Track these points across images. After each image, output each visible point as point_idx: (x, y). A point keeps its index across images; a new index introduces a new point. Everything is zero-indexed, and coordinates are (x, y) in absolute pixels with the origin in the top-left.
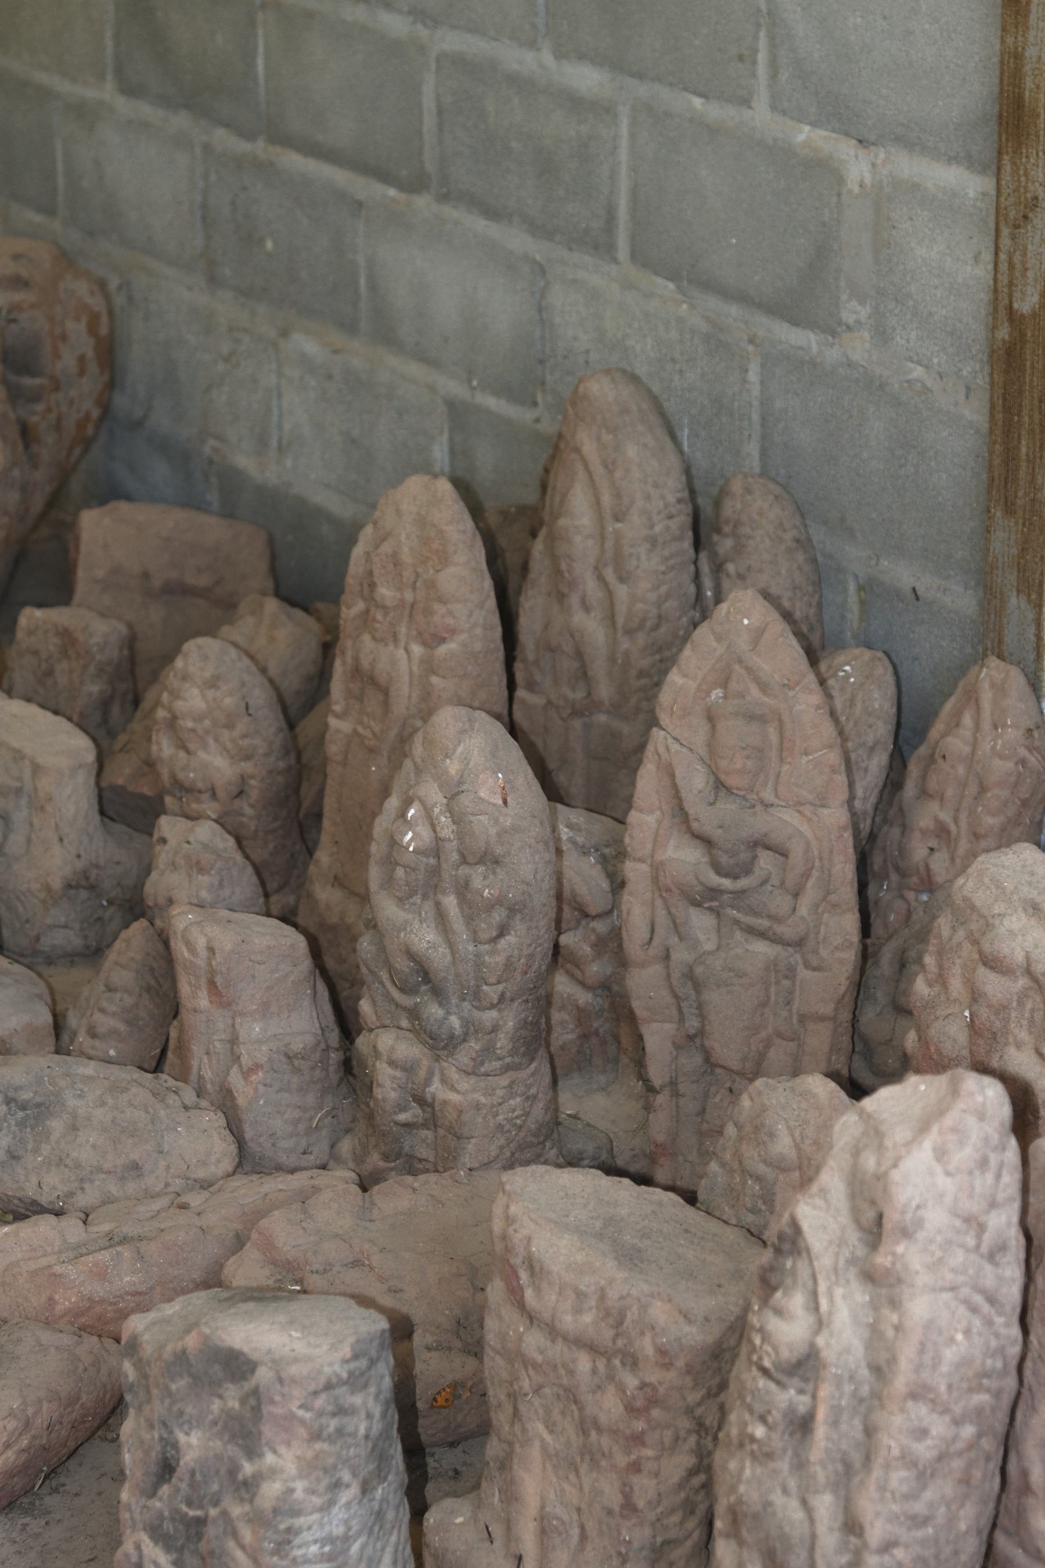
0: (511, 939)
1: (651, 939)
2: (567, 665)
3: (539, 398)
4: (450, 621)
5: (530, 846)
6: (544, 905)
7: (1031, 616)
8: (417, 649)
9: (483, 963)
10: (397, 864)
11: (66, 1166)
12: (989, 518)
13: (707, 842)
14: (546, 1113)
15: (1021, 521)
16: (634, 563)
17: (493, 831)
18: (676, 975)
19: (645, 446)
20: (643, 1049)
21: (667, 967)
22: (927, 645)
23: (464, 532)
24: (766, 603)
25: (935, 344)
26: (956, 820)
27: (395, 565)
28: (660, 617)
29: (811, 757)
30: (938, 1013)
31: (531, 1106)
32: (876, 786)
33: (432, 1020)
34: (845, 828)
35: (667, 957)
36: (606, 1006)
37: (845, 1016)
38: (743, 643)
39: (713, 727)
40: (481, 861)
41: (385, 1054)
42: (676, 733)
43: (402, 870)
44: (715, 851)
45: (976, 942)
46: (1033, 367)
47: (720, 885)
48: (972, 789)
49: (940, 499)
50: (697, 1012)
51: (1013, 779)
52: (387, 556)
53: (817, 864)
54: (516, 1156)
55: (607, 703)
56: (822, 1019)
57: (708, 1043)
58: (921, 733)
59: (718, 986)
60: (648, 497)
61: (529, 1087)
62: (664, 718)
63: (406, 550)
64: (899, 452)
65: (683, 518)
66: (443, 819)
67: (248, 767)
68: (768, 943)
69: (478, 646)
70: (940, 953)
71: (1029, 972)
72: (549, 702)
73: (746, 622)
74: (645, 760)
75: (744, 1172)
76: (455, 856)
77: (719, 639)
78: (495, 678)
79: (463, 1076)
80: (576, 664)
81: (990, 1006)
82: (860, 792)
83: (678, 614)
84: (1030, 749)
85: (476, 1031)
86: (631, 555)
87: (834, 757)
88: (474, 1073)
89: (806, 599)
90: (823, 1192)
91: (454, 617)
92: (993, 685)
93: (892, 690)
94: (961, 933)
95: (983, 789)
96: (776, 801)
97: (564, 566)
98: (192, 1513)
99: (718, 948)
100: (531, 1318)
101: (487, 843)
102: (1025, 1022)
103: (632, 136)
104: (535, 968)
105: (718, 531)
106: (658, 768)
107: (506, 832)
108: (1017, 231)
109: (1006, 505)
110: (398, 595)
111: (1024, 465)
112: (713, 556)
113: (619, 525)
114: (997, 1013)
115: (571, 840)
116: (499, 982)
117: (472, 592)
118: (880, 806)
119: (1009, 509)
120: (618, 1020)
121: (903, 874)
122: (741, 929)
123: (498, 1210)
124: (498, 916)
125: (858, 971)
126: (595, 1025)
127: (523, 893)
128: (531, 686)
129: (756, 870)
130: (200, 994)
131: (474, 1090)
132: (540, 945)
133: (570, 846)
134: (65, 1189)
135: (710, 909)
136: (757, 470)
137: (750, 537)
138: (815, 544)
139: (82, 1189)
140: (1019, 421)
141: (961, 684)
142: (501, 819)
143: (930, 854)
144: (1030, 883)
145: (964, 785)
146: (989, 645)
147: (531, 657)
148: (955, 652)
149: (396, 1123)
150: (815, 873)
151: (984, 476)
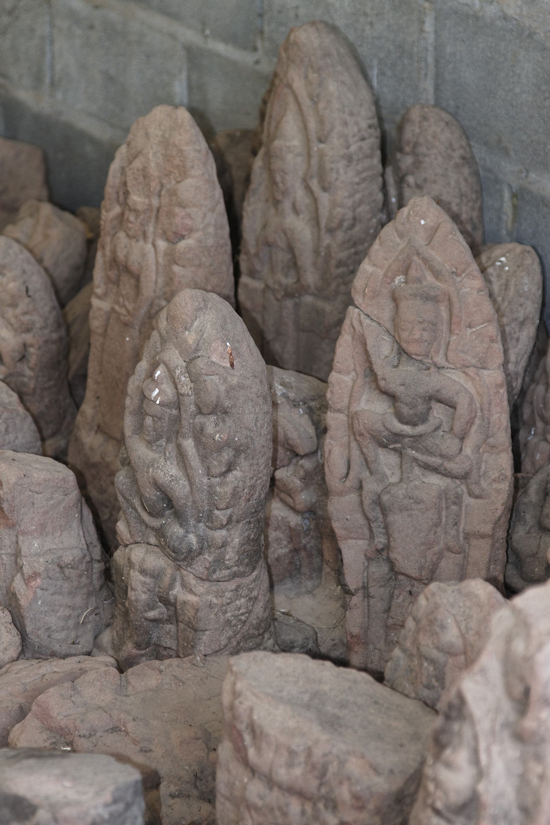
0: (237, 473)
1: (348, 473)
2: (282, 257)
4: (188, 222)
5: (252, 400)
6: (263, 446)
8: (162, 244)
9: (215, 492)
10: (147, 414)
13: (392, 397)
14: (265, 611)
16: (334, 175)
17: (222, 388)
18: (367, 502)
19: (343, 83)
20: (342, 560)
21: (361, 496)
23: (199, 151)
27: (144, 177)
28: (354, 219)
29: (474, 330)
32: (526, 353)
34: (501, 386)
35: (360, 487)
36: (312, 527)
37: (501, 534)
38: (420, 240)
39: (397, 306)
42: (368, 311)
43: (151, 418)
44: (398, 404)
50: (384, 531)
52: (138, 170)
53: (479, 414)
54: (241, 645)
57: (392, 556)
59: (401, 511)
60: (345, 124)
61: (251, 590)
62: (358, 299)
63: (153, 165)
65: (373, 140)
67: (28, 338)
69: (210, 242)
72: (267, 287)
73: (423, 222)
74: (343, 332)
75: (422, 657)
76: (193, 408)
78: (224, 268)
79: (199, 581)
83: (369, 216)
85: (209, 546)
86: (332, 169)
87: (492, 330)
88: (208, 580)
89: (470, 204)
90: (483, 671)
93: (538, 277)
96: (446, 364)
97: (278, 179)
99: (401, 480)
100: (253, 771)
101: (218, 397)
104: (255, 496)
107: (232, 389)
112: (397, 169)
113: (322, 146)
115: (284, 395)
116: (227, 508)
117: (206, 199)
118: (529, 369)
122: (419, 466)
123: (227, 686)
124: (227, 455)
125: (511, 499)
126: (304, 542)
128: (252, 274)
129: (431, 418)
131: (208, 593)
132: (260, 478)
133: (284, 400)
135: (395, 450)
136: (432, 102)
137: (425, 155)
138: (478, 160)
142: (229, 379)
147: (252, 251)
149: (146, 619)
150: (477, 421)
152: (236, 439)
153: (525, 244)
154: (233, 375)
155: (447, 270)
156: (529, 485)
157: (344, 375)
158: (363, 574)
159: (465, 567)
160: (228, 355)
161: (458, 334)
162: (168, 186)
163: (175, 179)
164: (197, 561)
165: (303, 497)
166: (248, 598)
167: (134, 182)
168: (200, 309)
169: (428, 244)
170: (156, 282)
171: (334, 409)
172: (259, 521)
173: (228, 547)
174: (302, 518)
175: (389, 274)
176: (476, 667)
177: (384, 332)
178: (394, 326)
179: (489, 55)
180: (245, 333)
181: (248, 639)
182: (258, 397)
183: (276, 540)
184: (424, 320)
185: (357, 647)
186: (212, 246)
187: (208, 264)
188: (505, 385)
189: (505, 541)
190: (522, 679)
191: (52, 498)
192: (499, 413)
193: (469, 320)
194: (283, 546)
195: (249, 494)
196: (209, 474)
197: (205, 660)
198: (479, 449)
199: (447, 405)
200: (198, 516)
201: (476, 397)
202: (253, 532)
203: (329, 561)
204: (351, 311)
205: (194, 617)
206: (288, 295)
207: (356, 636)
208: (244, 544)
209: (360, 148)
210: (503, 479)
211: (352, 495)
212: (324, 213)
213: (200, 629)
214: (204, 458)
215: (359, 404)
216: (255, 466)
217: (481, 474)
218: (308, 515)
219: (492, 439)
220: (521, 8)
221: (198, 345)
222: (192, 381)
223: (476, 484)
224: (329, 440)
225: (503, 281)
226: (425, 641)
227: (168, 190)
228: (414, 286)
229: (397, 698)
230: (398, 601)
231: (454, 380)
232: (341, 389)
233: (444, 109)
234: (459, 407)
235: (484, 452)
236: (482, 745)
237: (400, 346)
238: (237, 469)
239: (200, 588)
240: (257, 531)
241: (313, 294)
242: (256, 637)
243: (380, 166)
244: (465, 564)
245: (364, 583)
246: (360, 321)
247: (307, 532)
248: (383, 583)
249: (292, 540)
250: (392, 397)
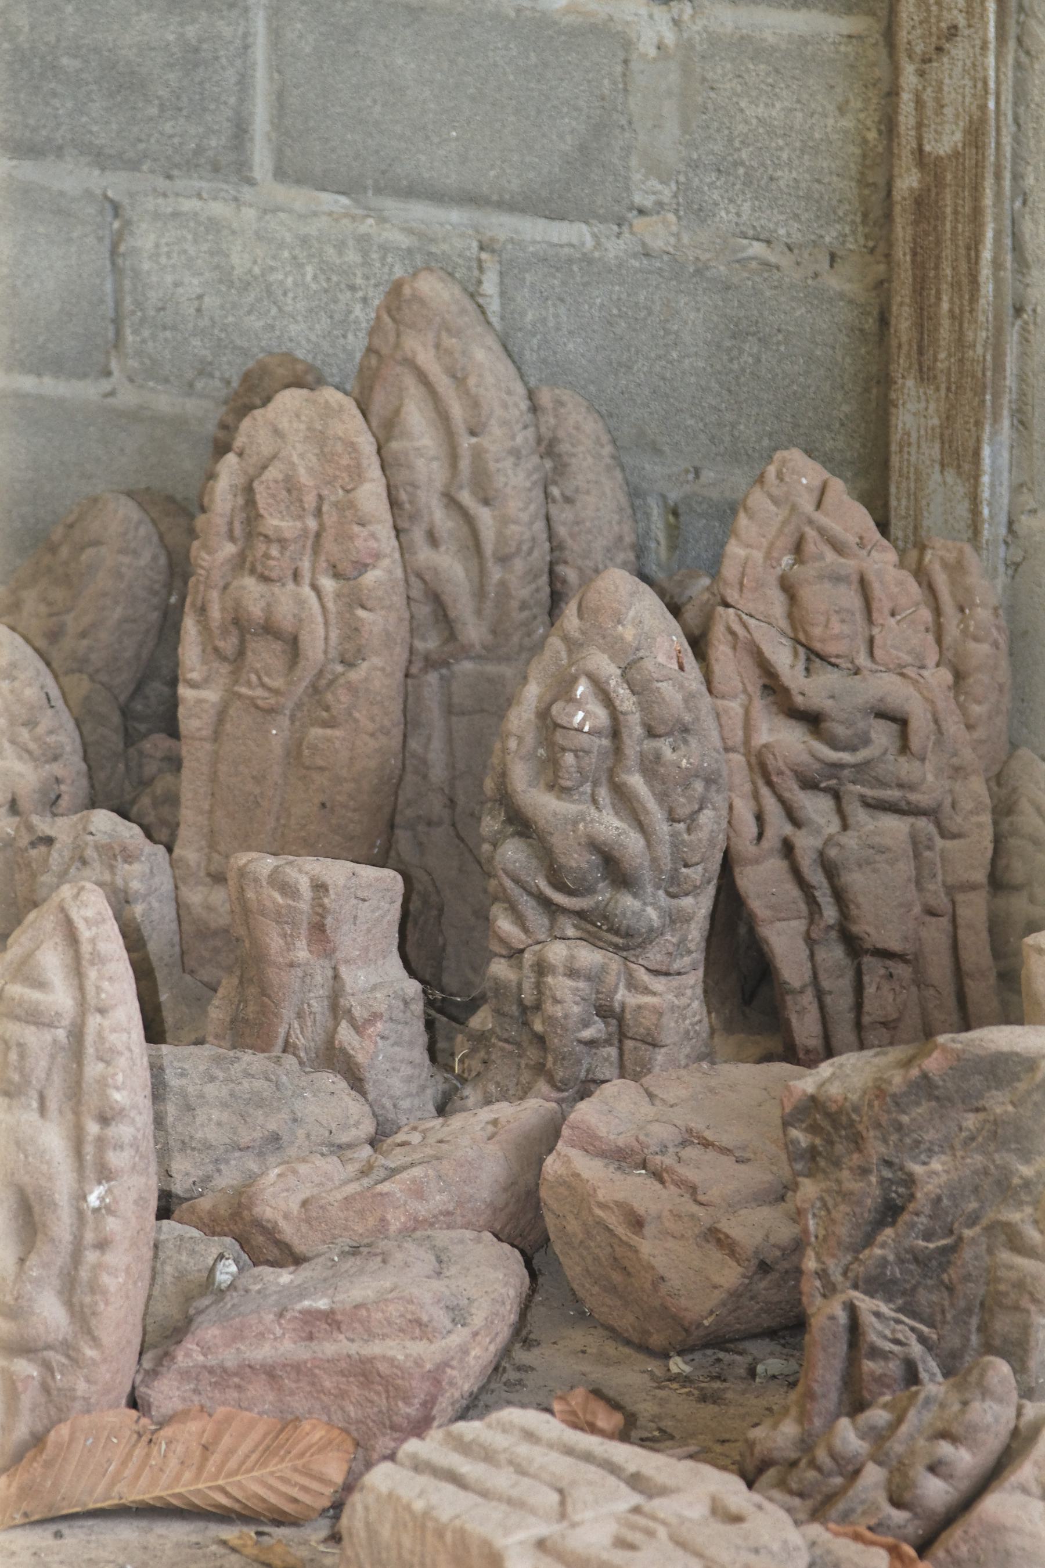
3: (114, 365)
8: (328, 584)
9: (683, 842)
10: (564, 749)
11: (193, 1149)
16: (503, 479)
25: (782, 213)
27: (289, 491)
33: (629, 914)
41: (560, 965)
42: (750, 607)
43: (572, 755)
46: (956, 212)
52: (276, 482)
55: (478, 647)
63: (302, 471)
66: (621, 691)
67: (57, 769)
74: (716, 643)
76: (639, 731)
86: (498, 470)
91: (377, 539)
92: (945, 565)
98: (931, 1246)
103: (276, 35)
108: (926, 66)
110: (299, 524)
111: (946, 323)
130: (298, 944)
134: (201, 1173)
139: (219, 1171)
149: (580, 1042)
162: (333, 498)
163: (342, 488)
167: (271, 501)
170: (326, 638)
191: (378, 908)
205: (656, 1026)
211: (772, 861)
214: (662, 797)
220: (677, 235)
222: (633, 693)
227: (335, 505)
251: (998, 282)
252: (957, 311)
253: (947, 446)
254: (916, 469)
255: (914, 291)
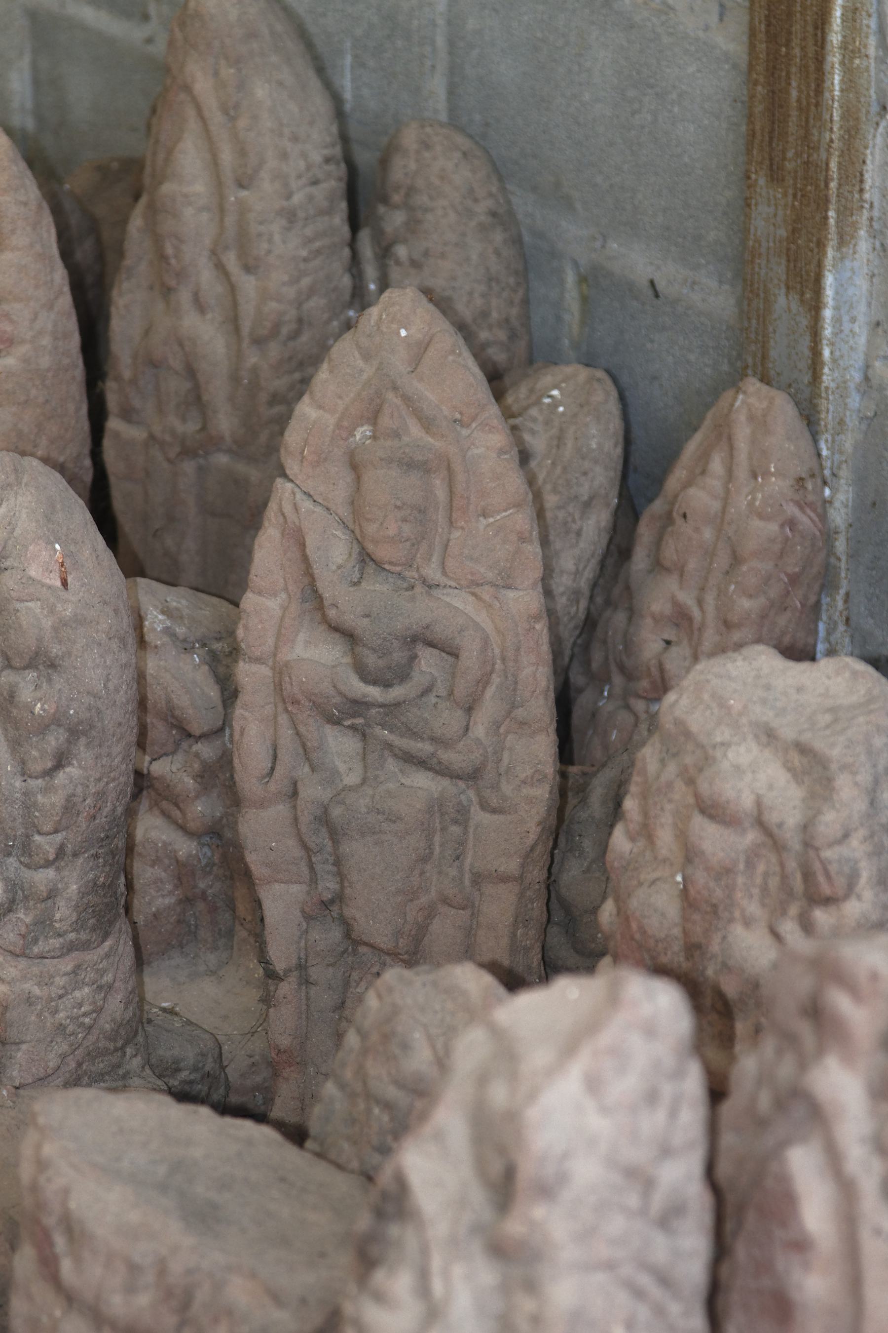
0: (72, 771)
1: (273, 769)
2: (176, 386)
5: (100, 644)
6: (120, 724)
7: (804, 322)
9: (35, 804)
12: (749, 187)
13: (349, 636)
14: (126, 1008)
15: (791, 191)
16: (265, 246)
17: (47, 623)
18: (305, 819)
19: (280, 83)
20: (262, 920)
21: (295, 807)
22: (670, 359)
23: (25, 204)
24: (431, 307)
26: (700, 602)
28: (300, 321)
29: (491, 520)
30: (642, 877)
31: (105, 999)
32: (593, 556)
34: (537, 618)
35: (295, 794)
36: (216, 858)
37: (537, 874)
38: (399, 363)
39: (358, 479)
40: (30, 666)
42: (309, 486)
44: (359, 649)
45: (691, 782)
47: (365, 696)
48: (722, 560)
49: (686, 160)
50: (335, 869)
51: (777, 547)
53: (499, 666)
54: (84, 1067)
56: (504, 879)
57: (348, 912)
58: (657, 482)
59: (363, 834)
60: (284, 156)
61: (102, 973)
62: (292, 467)
64: (631, 93)
65: (333, 183)
68: (430, 774)
69: (45, 362)
70: (644, 796)
71: (760, 823)
72: (152, 437)
73: (403, 333)
74: (266, 523)
75: (370, 1097)
77: (367, 357)
78: (71, 407)
79: (9, 958)
80: (188, 385)
81: (708, 869)
82: (567, 562)
83: (326, 316)
84: (801, 506)
85: (26, 898)
86: (260, 235)
87: (523, 520)
88: (23, 955)
89: (505, 294)
90: (439, 1136)
92: (751, 418)
93: (616, 424)
94: (672, 769)
95: (736, 560)
96: (443, 580)
97: (169, 250)
99: (364, 781)
100: (69, 1298)
101: (40, 640)
102: (756, 891)
104: (106, 811)
105: (385, 200)
106: (283, 535)
107: (65, 625)
109: (771, 170)
111: (794, 113)
112: (378, 234)
113: (244, 193)
114: (718, 878)
115: (167, 631)
116: (56, 831)
117: (37, 287)
118: (601, 581)
119: (776, 175)
120: (232, 878)
121: (629, 675)
122: (395, 756)
123: (27, 1150)
124: (55, 740)
125: (554, 813)
126: (202, 885)
127: (89, 709)
128: (127, 414)
129: (416, 675)
131: (24, 978)
132: (114, 780)
133: (166, 639)
135: (353, 728)
136: (443, 117)
137: (426, 210)
138: (520, 217)
140: (787, 54)
141: (710, 415)
142: (59, 607)
143: (666, 649)
144: (764, 702)
145: (710, 554)
146: (750, 361)
147: (127, 374)
148: (708, 371)
150: (496, 679)
151: (744, 128)
152: (72, 712)
153: (595, 367)
154: (66, 601)
155: (445, 417)
156: (590, 787)
157: (267, 598)
158: (299, 943)
159: (473, 932)
160: (57, 567)
161: (462, 528)
164: (5, 923)
165: (199, 808)
166: (95, 986)
168: (8, 485)
169: (412, 372)
171: (249, 658)
172: (113, 853)
173: (58, 899)
174: (199, 844)
175: (345, 424)
176: (428, 1129)
177: (336, 524)
178: (353, 513)
179: (539, 35)
180: (89, 526)
181: (96, 1057)
182: (110, 639)
183: (155, 883)
184: (404, 504)
185: (288, 1070)
186: (48, 370)
187: (41, 400)
188: (545, 615)
189: (543, 886)
190: (502, 1150)
192: (533, 664)
193: (482, 503)
194: (165, 892)
195: (94, 807)
196: (25, 774)
197: (17, 1095)
198: (499, 727)
199: (444, 651)
200: (6, 845)
201: (495, 639)
202: (103, 872)
203: (244, 919)
204: (279, 486)
206: (187, 452)
207: (285, 1052)
208: (88, 894)
209: (311, 198)
210: (538, 780)
211: (281, 807)
212: (248, 310)
213: (12, 1040)
215: (292, 648)
216: (105, 759)
217: (502, 770)
218: (208, 839)
219: (521, 709)
221: (4, 547)
223: (493, 788)
224: (242, 711)
225: (554, 431)
226: (376, 1069)
228: (389, 443)
229: (321, 1172)
230: (358, 990)
231: (456, 608)
232: (261, 622)
233: (461, 130)
234: (464, 655)
235: (508, 732)
236: (436, 1262)
237: (363, 549)
238: (73, 765)
239: (11, 970)
240: (110, 870)
241: (229, 451)
242: (112, 1054)
243: (346, 230)
244: (474, 927)
245: (299, 958)
246: (295, 504)
247: (208, 869)
248: (332, 960)
249: (181, 883)
250: (349, 636)
251: (849, 73)
252: (804, 103)
253: (792, 265)
254: (765, 286)
255: (767, 70)
